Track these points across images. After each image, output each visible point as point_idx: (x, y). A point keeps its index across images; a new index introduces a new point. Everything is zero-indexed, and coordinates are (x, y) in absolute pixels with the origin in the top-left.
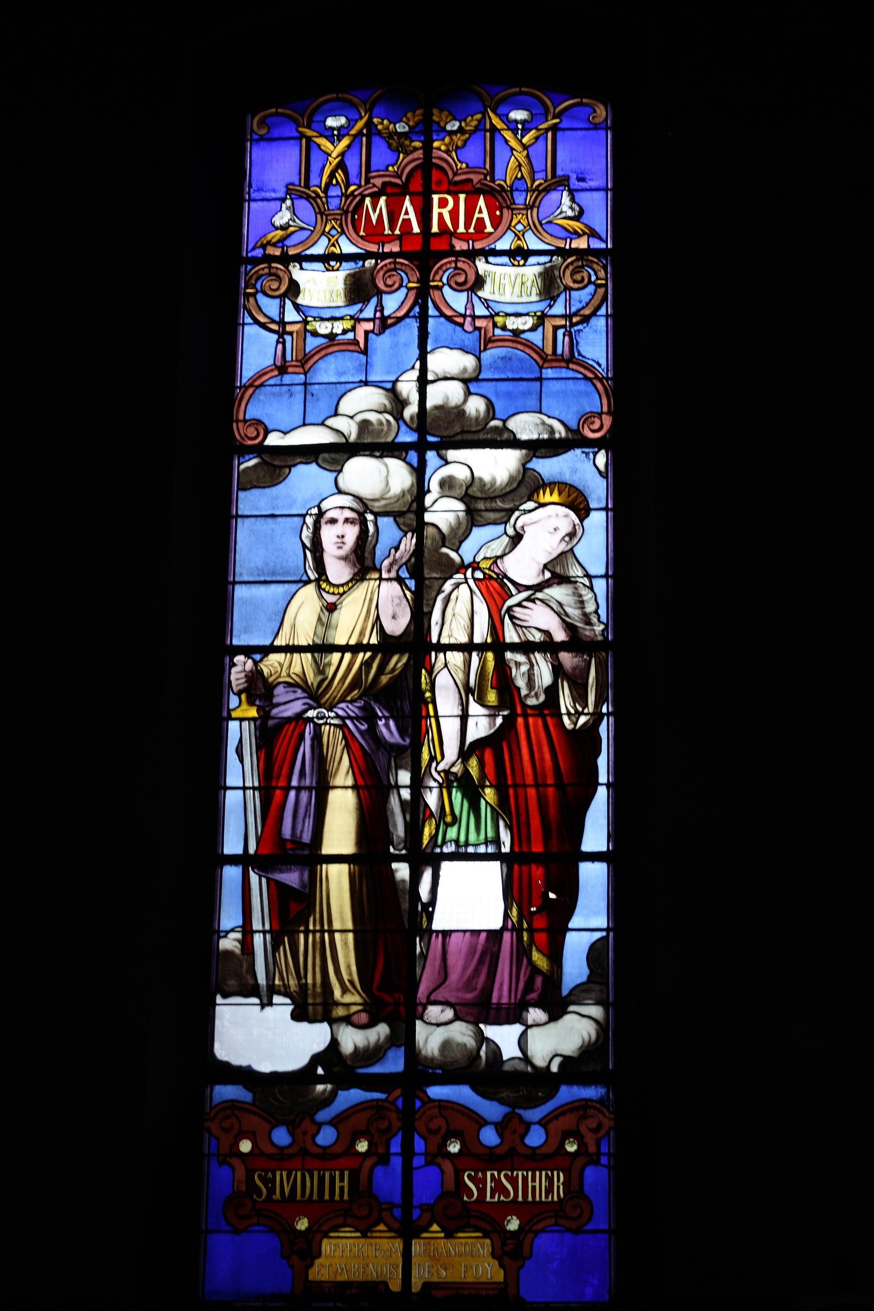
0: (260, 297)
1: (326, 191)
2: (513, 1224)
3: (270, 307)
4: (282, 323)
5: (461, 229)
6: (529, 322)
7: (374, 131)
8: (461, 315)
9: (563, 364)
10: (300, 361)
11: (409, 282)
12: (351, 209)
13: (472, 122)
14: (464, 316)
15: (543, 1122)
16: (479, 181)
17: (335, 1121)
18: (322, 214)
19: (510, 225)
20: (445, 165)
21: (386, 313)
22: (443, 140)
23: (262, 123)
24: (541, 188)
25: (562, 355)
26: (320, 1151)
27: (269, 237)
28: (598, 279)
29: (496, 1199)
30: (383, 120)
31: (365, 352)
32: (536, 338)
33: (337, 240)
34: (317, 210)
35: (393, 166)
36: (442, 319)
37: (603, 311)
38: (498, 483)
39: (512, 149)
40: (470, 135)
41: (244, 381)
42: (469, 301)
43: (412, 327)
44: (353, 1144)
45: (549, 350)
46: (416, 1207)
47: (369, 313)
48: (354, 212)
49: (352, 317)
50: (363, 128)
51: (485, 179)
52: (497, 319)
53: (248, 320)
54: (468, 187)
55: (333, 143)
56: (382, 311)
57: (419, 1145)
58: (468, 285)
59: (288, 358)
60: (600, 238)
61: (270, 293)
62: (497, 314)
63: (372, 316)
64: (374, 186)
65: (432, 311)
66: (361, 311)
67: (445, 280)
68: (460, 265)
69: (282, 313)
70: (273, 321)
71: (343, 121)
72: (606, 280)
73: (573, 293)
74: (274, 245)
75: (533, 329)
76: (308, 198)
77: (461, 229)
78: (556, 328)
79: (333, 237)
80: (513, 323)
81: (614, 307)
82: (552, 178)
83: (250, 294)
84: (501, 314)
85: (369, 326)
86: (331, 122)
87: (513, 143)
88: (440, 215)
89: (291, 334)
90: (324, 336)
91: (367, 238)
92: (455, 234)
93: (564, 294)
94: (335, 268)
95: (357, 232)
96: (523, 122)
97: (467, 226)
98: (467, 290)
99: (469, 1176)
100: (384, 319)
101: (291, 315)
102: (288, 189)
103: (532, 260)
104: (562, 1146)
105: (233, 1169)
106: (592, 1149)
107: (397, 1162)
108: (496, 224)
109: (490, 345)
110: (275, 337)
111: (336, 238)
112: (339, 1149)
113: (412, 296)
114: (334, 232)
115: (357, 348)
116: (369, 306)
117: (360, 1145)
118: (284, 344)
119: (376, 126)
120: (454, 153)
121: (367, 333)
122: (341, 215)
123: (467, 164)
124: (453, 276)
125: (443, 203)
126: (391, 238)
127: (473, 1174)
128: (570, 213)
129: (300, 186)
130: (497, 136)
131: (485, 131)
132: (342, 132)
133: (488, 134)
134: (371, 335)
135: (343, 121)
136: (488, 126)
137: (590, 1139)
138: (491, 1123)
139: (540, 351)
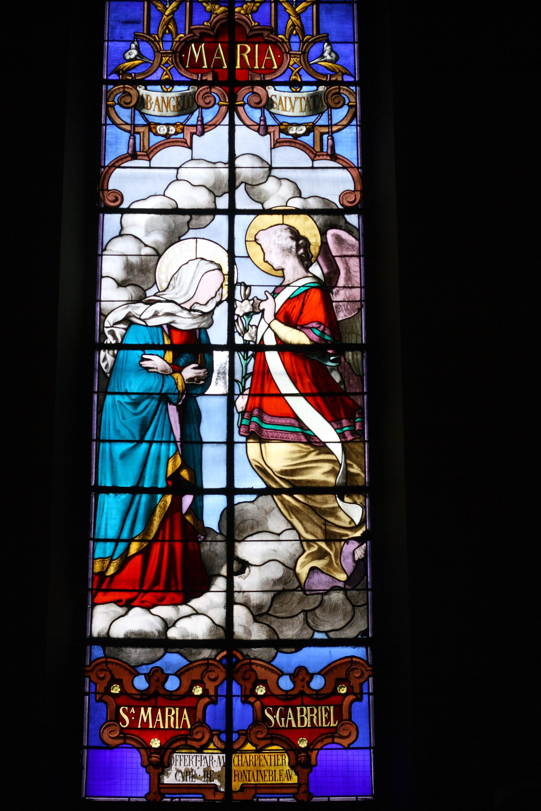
0: (246, 106)
1: (289, 39)
2: (156, 743)
3: (125, 114)
4: (134, 125)
6: (304, 129)
10: (146, 152)
11: (220, 101)
12: (179, 50)
14: (259, 125)
15: (322, 673)
16: (268, 36)
17: (179, 673)
19: (160, 64)
20: (244, 24)
22: (242, 6)
24: (310, 41)
25: (327, 152)
26: (284, 693)
27: (122, 66)
28: (220, 101)
29: (328, 725)
31: (191, 147)
34: (156, 50)
35: (207, 22)
36: (244, 127)
37: (354, 122)
38: (290, 235)
39: (290, 15)
41: (106, 164)
42: (263, 114)
44: (191, 688)
46: (235, 732)
47: (193, 120)
48: (181, 52)
49: (182, 124)
53: (109, 122)
56: (202, 120)
57: (236, 689)
58: (261, 105)
59: (138, 149)
60: (351, 75)
61: (125, 105)
63: (195, 123)
64: (195, 35)
65: (237, 121)
66: (188, 119)
67: (116, 101)
68: (255, 90)
69: (133, 118)
70: (127, 124)
72: (356, 102)
75: (306, 134)
76: (148, 41)
77: (257, 67)
80: (293, 130)
81: (361, 121)
82: (189, 33)
84: (284, 124)
85: (194, 130)
87: (290, 11)
88: (242, 58)
89: (139, 133)
90: (162, 136)
91: (190, 70)
92: (253, 70)
93: (327, 111)
94: (169, 90)
95: (184, 66)
99: (124, 710)
100: (203, 125)
101: (139, 120)
102: (135, 35)
103: (305, 88)
104: (335, 690)
105: (106, 704)
106: (212, 693)
107: (222, 702)
108: (280, 63)
109: (277, 145)
110: (128, 135)
111: (297, 70)
112: (328, 691)
113: (224, 109)
115: (186, 145)
116: (193, 116)
117: (196, 690)
118: (135, 139)
120: (250, 15)
124: (121, 98)
126: (205, 72)
127: (127, 708)
128: (328, 58)
129: (143, 33)
130: (279, 6)
133: (273, 5)
134: (195, 137)
137: (105, 683)
138: (286, 674)
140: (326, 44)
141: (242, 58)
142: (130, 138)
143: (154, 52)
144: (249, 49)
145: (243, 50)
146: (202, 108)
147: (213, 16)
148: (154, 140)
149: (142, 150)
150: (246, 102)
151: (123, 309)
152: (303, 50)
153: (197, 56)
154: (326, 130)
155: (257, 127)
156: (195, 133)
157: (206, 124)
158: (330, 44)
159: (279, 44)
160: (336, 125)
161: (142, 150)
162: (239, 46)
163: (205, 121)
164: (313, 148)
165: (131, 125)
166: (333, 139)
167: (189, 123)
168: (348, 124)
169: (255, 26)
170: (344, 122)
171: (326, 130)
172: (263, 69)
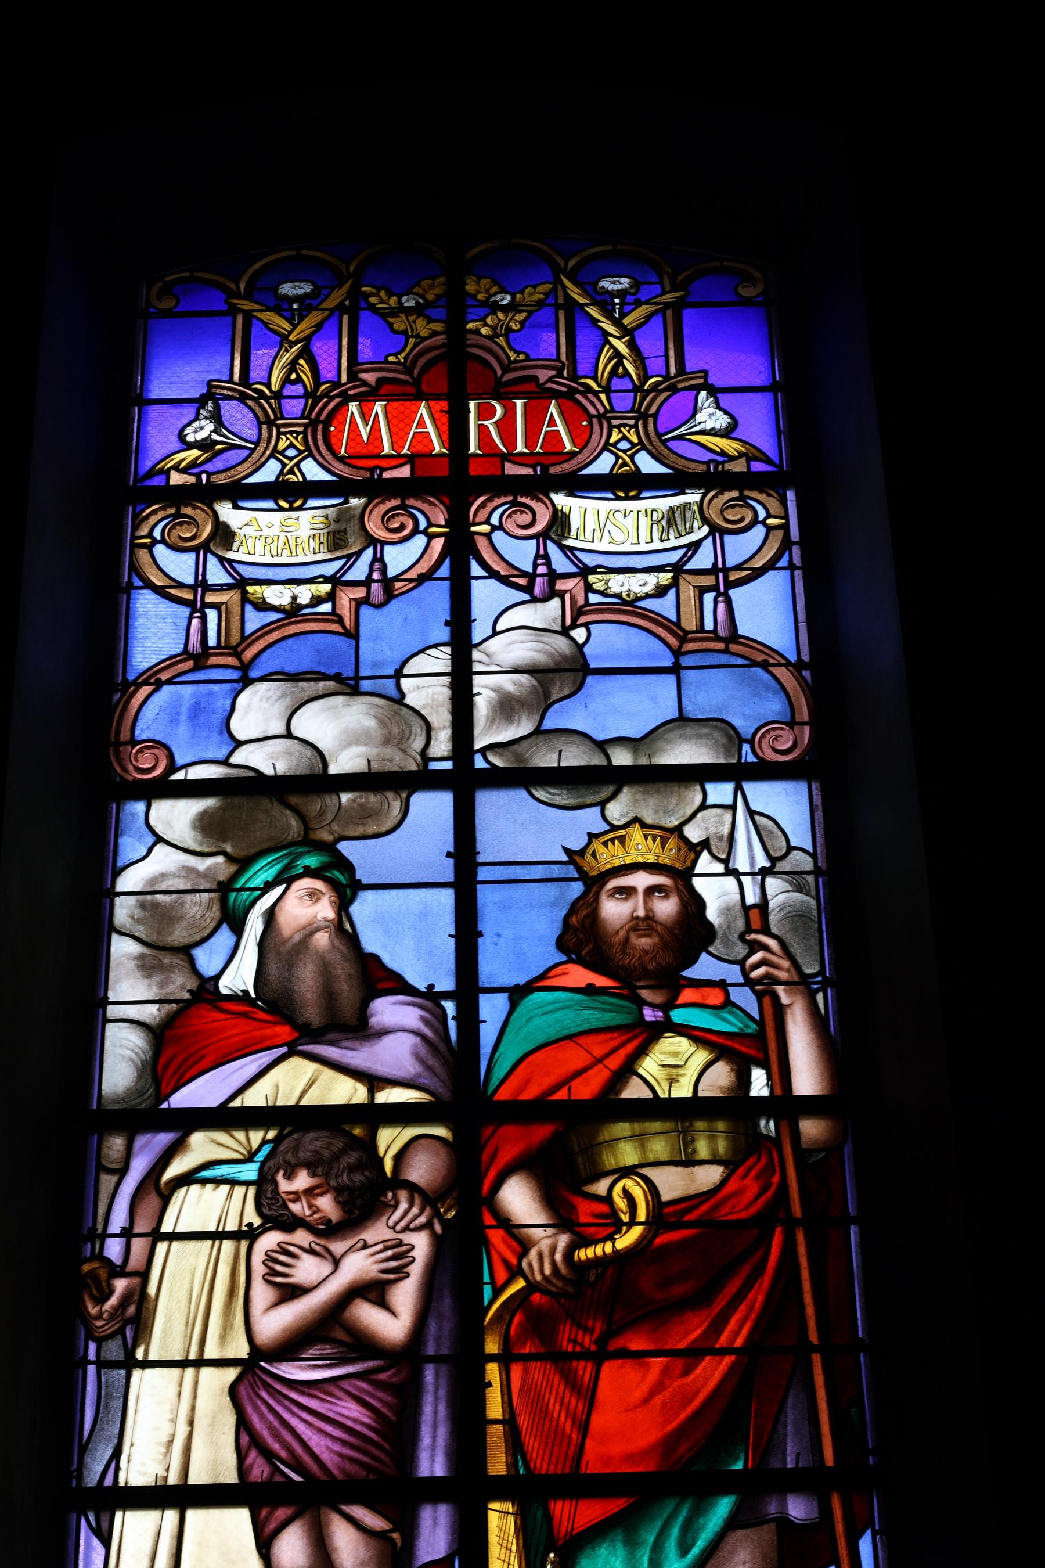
3: (180, 566)
4: (202, 585)
5: (521, 447)
7: (363, 305)
8: (523, 574)
9: (721, 646)
11: (769, 516)
13: (532, 296)
14: (532, 577)
18: (271, 424)
21: (391, 573)
22: (483, 319)
23: (167, 290)
30: (379, 291)
32: (666, 606)
33: (298, 465)
34: (262, 418)
35: (396, 354)
36: (492, 581)
39: (606, 334)
40: (530, 313)
43: (437, 597)
45: (689, 623)
47: (359, 571)
50: (345, 300)
51: (560, 375)
52: (592, 578)
53: (137, 582)
54: (531, 387)
55: (290, 321)
56: (384, 569)
59: (212, 642)
61: (181, 544)
62: (593, 570)
65: (476, 569)
66: (345, 570)
67: (157, 534)
70: (180, 585)
71: (306, 288)
72: (786, 517)
73: (727, 538)
74: (184, 471)
76: (242, 398)
77: (521, 447)
78: (702, 591)
79: (291, 459)
82: (349, 381)
83: (143, 546)
85: (360, 593)
86: (287, 289)
96: (621, 294)
97: (530, 442)
98: (195, 549)
100: (388, 583)
101: (216, 574)
114: (291, 453)
118: (204, 619)
119: (474, 297)
121: (359, 603)
122: (637, 419)
123: (526, 354)
125: (489, 413)
128: (709, 425)
131: (557, 307)
132: (307, 304)
134: (365, 611)
135: (306, 288)
136: (561, 300)
139: (675, 626)
140: (703, 394)
141: (482, 430)
142: (191, 618)
143: (260, 424)
144: (499, 411)
145: (489, 413)
146: (724, 532)
147: (412, 341)
148: (254, 620)
149: (223, 644)
150: (159, 538)
151: (395, 1003)
152: (313, 416)
153: (364, 432)
154: (709, 580)
155: (522, 581)
156: (366, 601)
157: (396, 578)
158: (713, 391)
159: (578, 396)
160: (738, 568)
161: (223, 644)
162: (472, 405)
163: (391, 573)
164: (678, 623)
165: (193, 588)
166: (729, 602)
167: (349, 577)
168: (771, 566)
169: (516, 361)
170: (759, 563)
171: (709, 580)
172: (538, 453)
